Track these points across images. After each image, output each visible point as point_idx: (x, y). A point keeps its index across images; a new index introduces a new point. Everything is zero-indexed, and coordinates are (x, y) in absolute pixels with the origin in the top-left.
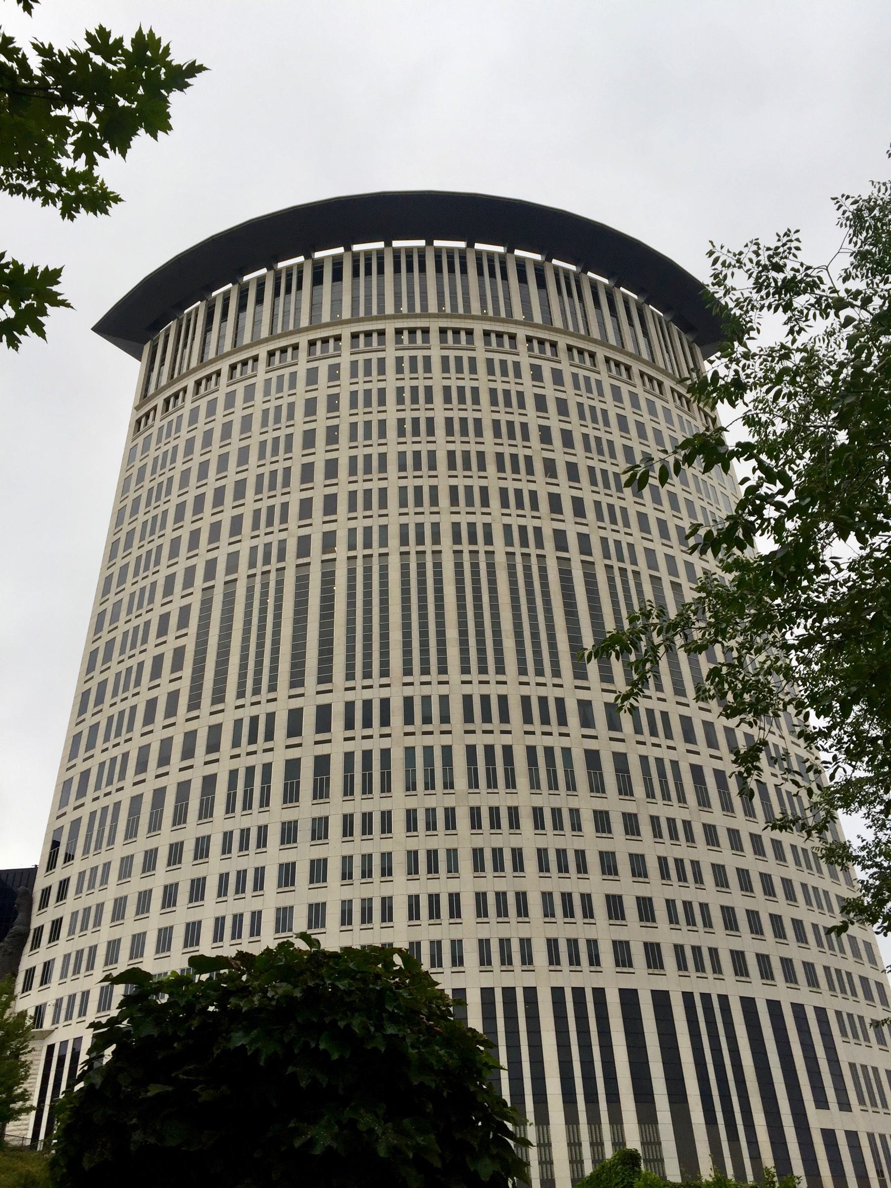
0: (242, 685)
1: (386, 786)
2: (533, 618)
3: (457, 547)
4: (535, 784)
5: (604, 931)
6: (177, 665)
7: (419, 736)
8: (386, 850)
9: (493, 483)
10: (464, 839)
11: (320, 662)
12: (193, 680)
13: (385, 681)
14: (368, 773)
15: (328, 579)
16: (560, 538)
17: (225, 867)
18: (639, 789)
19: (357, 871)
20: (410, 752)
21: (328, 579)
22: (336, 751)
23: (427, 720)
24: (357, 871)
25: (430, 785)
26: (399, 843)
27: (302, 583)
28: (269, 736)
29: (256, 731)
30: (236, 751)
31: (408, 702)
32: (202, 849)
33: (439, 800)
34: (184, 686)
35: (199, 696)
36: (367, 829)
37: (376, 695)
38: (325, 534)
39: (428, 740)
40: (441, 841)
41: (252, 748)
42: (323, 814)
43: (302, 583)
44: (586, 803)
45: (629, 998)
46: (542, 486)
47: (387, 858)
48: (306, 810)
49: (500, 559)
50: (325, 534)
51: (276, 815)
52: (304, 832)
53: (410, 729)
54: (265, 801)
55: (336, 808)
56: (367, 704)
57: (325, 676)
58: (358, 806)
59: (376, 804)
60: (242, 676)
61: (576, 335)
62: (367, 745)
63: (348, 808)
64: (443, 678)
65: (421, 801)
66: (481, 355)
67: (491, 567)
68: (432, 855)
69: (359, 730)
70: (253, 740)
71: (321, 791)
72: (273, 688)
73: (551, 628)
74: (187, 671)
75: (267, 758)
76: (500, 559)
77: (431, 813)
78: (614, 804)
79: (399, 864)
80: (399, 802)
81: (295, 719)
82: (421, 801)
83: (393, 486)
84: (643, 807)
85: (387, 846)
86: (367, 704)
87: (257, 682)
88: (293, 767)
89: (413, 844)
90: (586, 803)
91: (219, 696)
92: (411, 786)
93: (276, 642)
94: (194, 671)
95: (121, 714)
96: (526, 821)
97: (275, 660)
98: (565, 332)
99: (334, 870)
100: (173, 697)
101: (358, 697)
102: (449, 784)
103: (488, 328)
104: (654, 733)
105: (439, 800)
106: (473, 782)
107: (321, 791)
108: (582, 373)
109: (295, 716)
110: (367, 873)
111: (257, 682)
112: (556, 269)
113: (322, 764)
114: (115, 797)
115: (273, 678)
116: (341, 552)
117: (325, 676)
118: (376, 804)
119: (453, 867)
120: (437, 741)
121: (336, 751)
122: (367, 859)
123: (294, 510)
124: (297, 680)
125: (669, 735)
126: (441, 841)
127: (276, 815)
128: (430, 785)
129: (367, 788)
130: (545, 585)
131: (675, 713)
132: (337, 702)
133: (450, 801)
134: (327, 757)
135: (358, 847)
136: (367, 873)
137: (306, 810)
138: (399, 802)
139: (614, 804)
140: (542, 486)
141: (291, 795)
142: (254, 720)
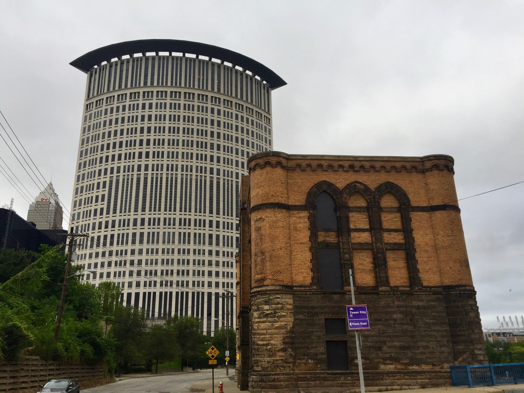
0: (121, 209)
1: (158, 242)
2: (201, 193)
3: (182, 173)
4: (195, 243)
5: (206, 279)
6: (104, 187)
7: (167, 229)
8: (156, 258)
9: (196, 104)
10: (176, 257)
11: (143, 205)
12: (109, 192)
13: (159, 213)
14: (153, 238)
15: (146, 179)
16: (212, 170)
17: (115, 270)
18: (221, 244)
19: (149, 263)
20: (164, 233)
21: (146, 179)
22: (146, 231)
23: (169, 225)
24: (149, 263)
25: (169, 242)
26: (160, 257)
27: (138, 180)
28: (128, 225)
29: (124, 223)
30: (125, 161)
31: (170, 128)
32: (111, 254)
33: (171, 246)
34: (105, 207)
35: (109, 211)
36: (152, 253)
37: (161, 138)
38: (145, 165)
39: (169, 230)
40: (170, 257)
41: (124, 228)
42: (141, 248)
43: (138, 180)
44: (207, 248)
45: (210, 294)
46: (209, 117)
47: (157, 260)
48: (137, 247)
49: (194, 177)
50: (145, 165)
51: (130, 247)
52: (137, 252)
53: (165, 227)
54: (127, 243)
55: (145, 247)
56: (154, 219)
57: (144, 210)
58: (150, 247)
59: (155, 247)
60: (121, 207)
61: (258, 107)
62: (160, 125)
63: (148, 247)
64: (174, 227)
65: (166, 246)
66: (196, 104)
67: (191, 179)
68: (168, 260)
69: (157, 133)
70: (124, 226)
71: (141, 242)
72: (129, 211)
73: (205, 199)
74: (106, 202)
75: (128, 231)
76: (194, 177)
77: (168, 249)
78: (214, 248)
79: (160, 262)
80: (160, 246)
81: (142, 129)
82: (166, 246)
83: (158, 280)
84: (221, 249)
85: (157, 257)
86: (154, 219)
87: (125, 209)
88: (134, 235)
89: (163, 257)
90: (207, 248)
91: (115, 212)
92: (164, 242)
93: (131, 195)
94: (109, 189)
95: (97, 123)
96: (192, 252)
97: (131, 198)
98: (255, 106)
99: (144, 251)
100: (102, 209)
101: (156, 150)
102: (173, 242)
103: (199, 93)
104: (228, 117)
105: (171, 246)
106: (180, 242)
107: (141, 242)
108: (259, 121)
109: (135, 220)
110: (151, 264)
111: (125, 209)
112: (256, 79)
113: (142, 234)
114: (97, 144)
115: (130, 209)
116: (150, 172)
117: (144, 210)
118: (155, 247)
119: (172, 263)
120: (172, 231)
121: (146, 231)
122: (152, 260)
123: (137, 155)
124: (136, 210)
125: (232, 129)
126: (170, 257)
127: (130, 247)
128: (169, 242)
129: (153, 242)
130: (205, 185)
131: (234, 136)
132: (152, 139)
133: (173, 247)
134: (144, 219)
135: (150, 257)
136: (151, 264)
137: (137, 247)
138: (160, 246)
139: (214, 248)
140: (209, 117)
141: (134, 242)
142: (124, 220)
